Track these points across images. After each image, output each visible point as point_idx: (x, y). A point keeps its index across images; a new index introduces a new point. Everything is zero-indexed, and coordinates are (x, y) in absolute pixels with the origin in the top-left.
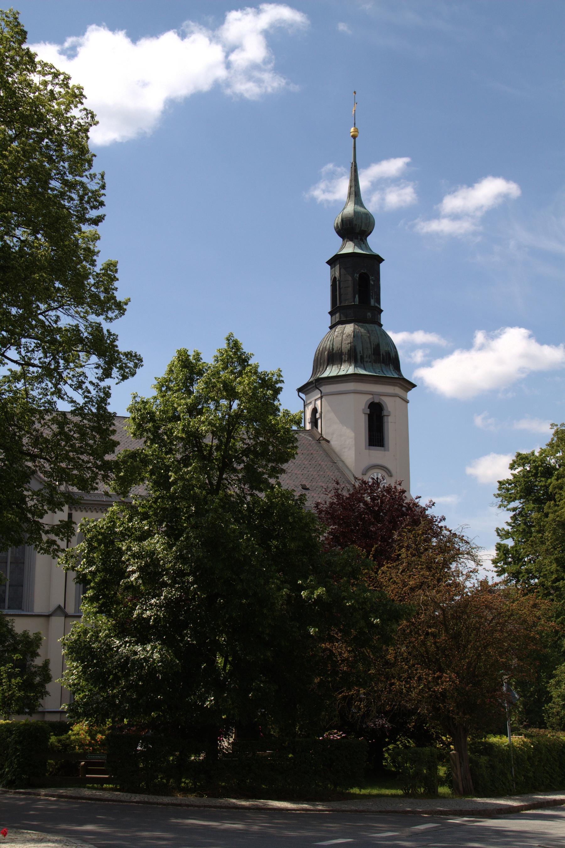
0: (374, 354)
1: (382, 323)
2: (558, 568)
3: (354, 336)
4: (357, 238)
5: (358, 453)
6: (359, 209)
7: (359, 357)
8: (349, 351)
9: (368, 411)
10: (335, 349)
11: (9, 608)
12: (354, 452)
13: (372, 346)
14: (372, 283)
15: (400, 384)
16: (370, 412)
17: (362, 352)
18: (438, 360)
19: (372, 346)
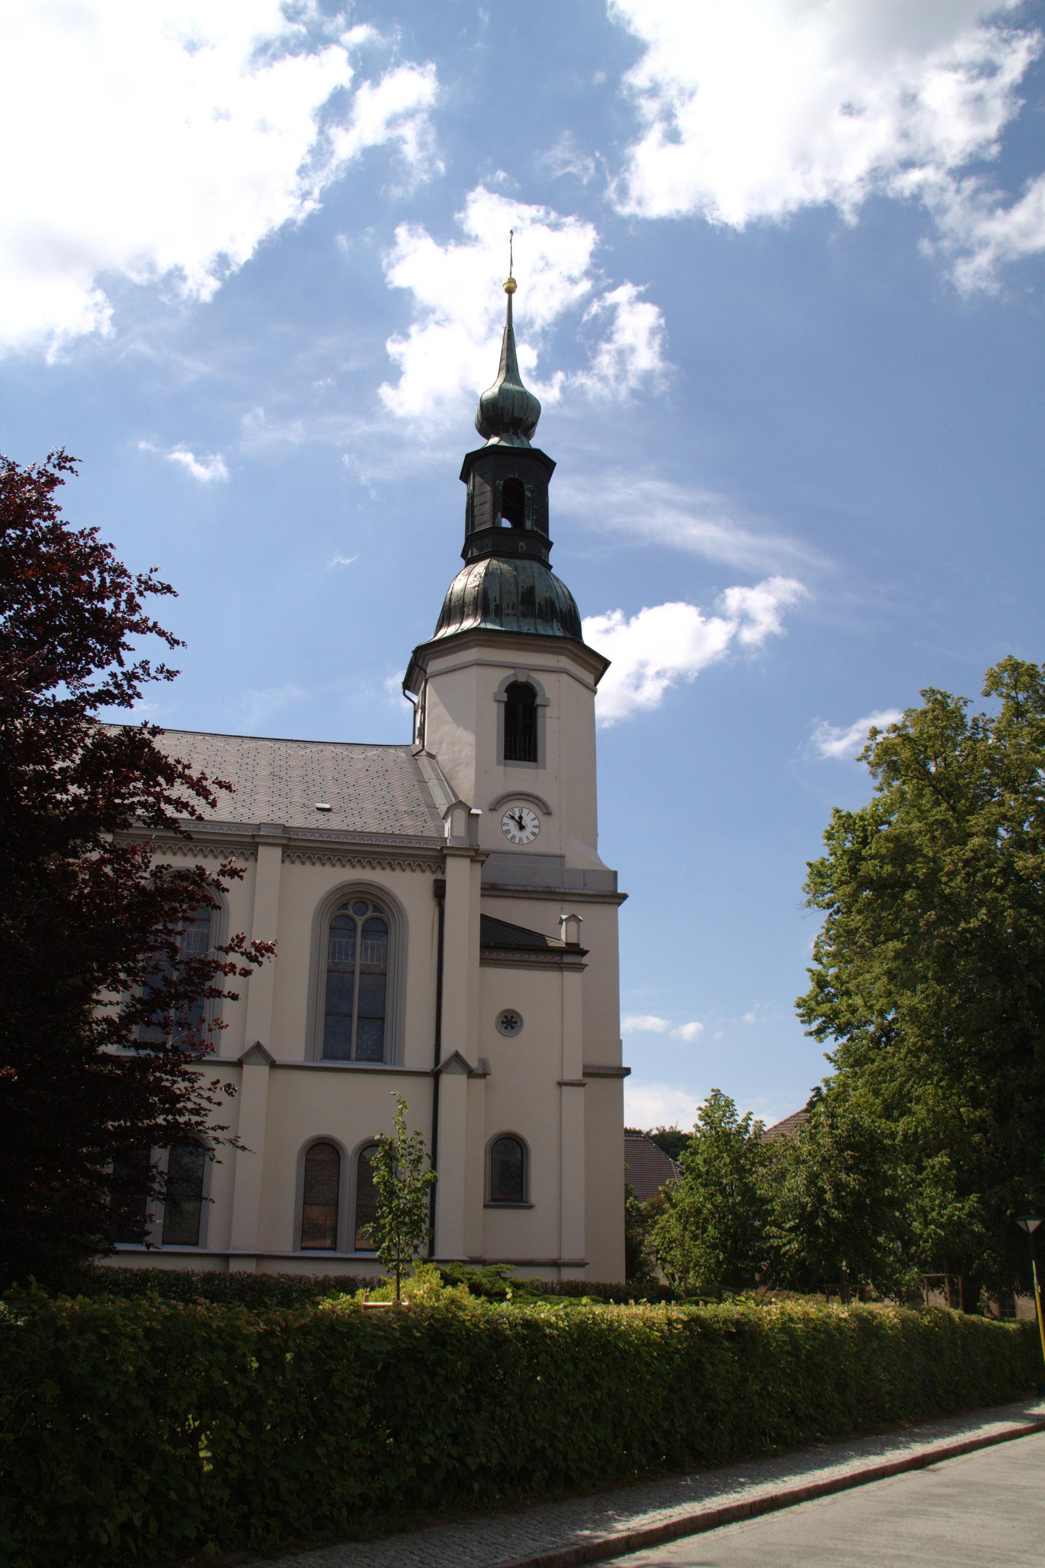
0: (522, 603)
1: (551, 563)
2: (891, 987)
3: (486, 575)
4: (507, 431)
5: (481, 771)
6: (510, 386)
7: (492, 606)
8: (476, 598)
9: (504, 697)
10: (454, 598)
11: (358, 1059)
12: (474, 770)
13: (520, 590)
14: (529, 495)
15: (569, 650)
16: (508, 697)
17: (498, 599)
18: (379, 144)
19: (520, 590)
